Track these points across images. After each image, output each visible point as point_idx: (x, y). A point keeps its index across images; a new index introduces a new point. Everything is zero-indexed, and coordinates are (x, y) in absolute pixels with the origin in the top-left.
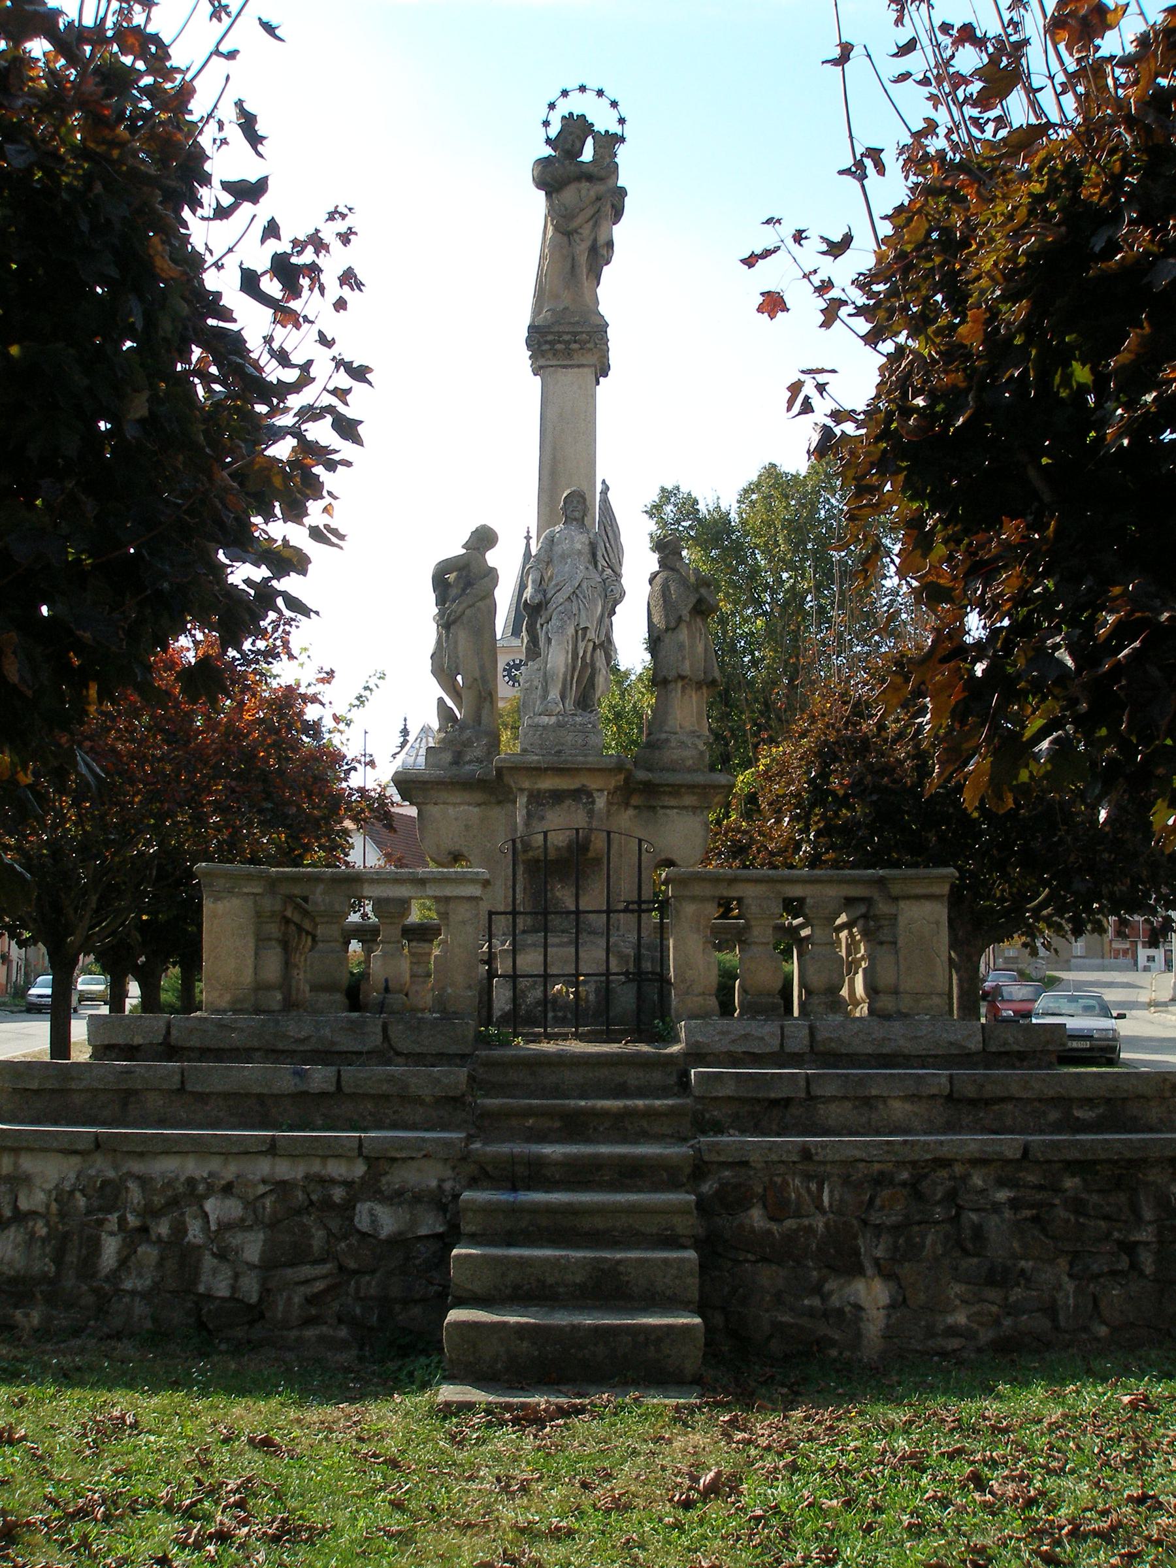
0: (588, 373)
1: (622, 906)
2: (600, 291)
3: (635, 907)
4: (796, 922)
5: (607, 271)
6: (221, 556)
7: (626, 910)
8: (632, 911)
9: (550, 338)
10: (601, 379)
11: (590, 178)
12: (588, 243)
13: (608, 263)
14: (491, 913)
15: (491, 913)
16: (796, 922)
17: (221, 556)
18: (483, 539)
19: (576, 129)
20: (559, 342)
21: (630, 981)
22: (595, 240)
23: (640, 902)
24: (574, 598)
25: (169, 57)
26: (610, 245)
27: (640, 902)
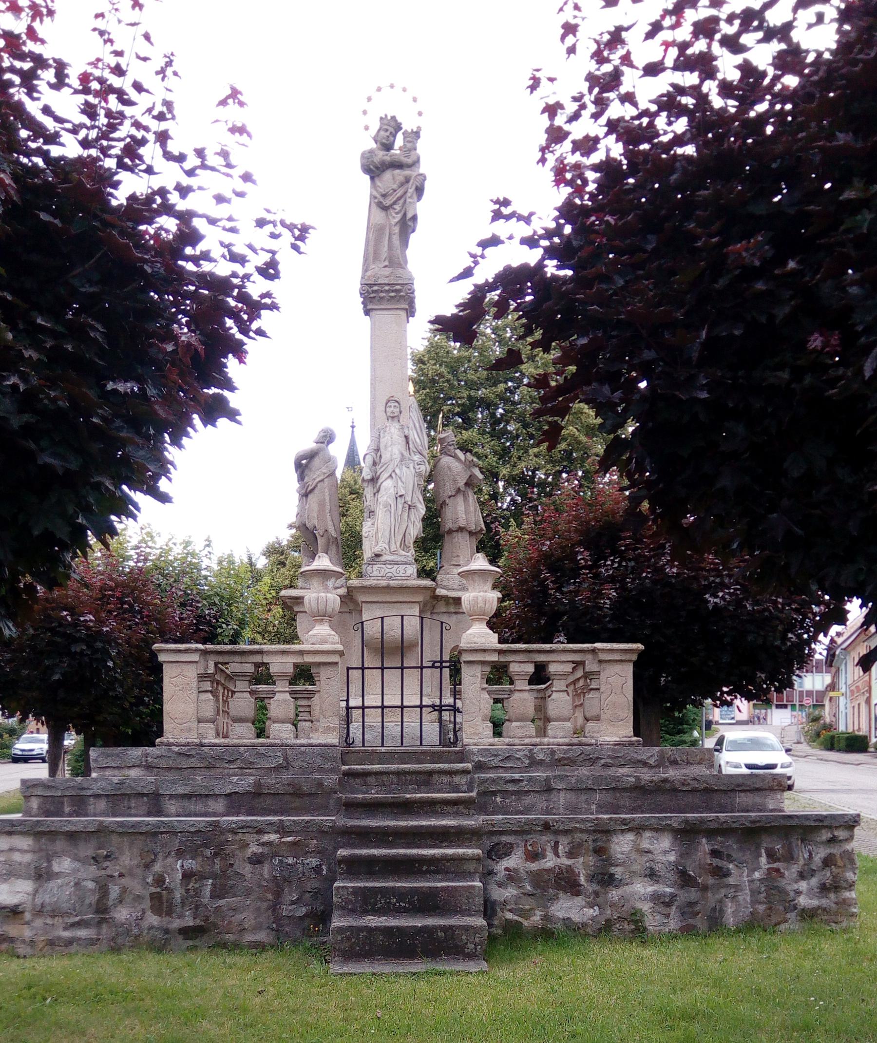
0: (403, 314)
1: (430, 664)
2: (409, 252)
3: (438, 664)
4: (502, 426)
5: (413, 237)
6: (625, 167)
7: (433, 667)
8: (437, 667)
9: (376, 288)
10: (411, 319)
11: (399, 165)
12: (399, 216)
13: (413, 231)
14: (348, 669)
15: (348, 669)
16: (502, 426)
17: (625, 167)
18: (327, 438)
19: (391, 126)
20: (382, 291)
21: (435, 710)
22: (405, 214)
23: (441, 662)
24: (393, 475)
25: (117, 98)
26: (414, 218)
27: (441, 662)
